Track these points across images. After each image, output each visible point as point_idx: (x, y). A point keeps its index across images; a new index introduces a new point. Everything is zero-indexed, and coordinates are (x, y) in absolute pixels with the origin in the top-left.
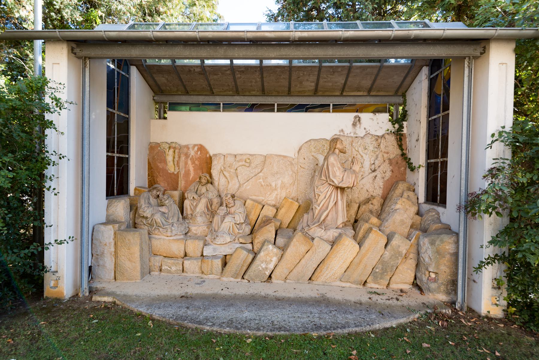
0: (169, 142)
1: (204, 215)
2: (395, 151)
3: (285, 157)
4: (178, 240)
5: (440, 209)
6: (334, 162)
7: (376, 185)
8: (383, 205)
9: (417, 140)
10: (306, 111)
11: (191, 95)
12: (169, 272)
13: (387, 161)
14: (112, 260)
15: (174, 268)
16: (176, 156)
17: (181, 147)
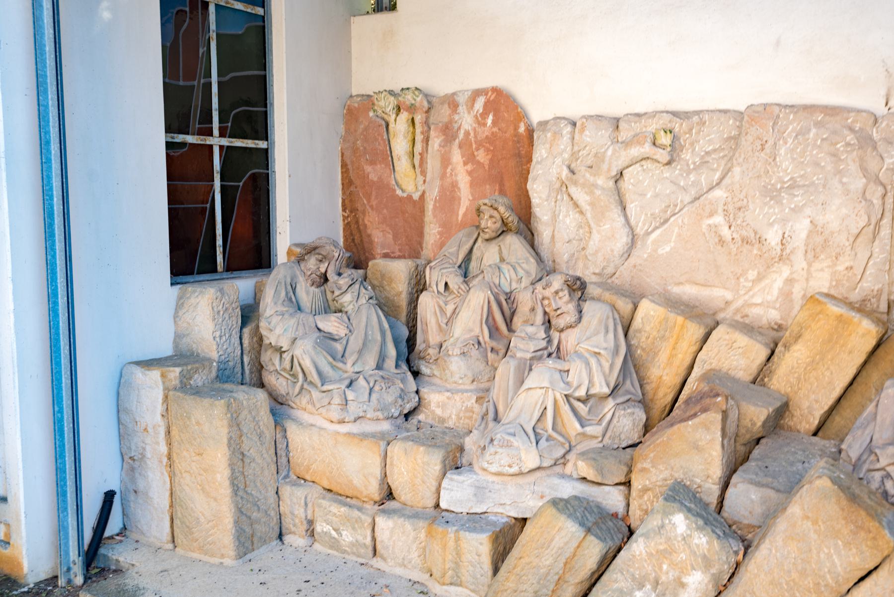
0: (397, 88)
1: (475, 353)
3: (831, 111)
4: (364, 436)
12: (334, 544)
14: (165, 482)
15: (347, 537)
16: (419, 138)
17: (431, 103)
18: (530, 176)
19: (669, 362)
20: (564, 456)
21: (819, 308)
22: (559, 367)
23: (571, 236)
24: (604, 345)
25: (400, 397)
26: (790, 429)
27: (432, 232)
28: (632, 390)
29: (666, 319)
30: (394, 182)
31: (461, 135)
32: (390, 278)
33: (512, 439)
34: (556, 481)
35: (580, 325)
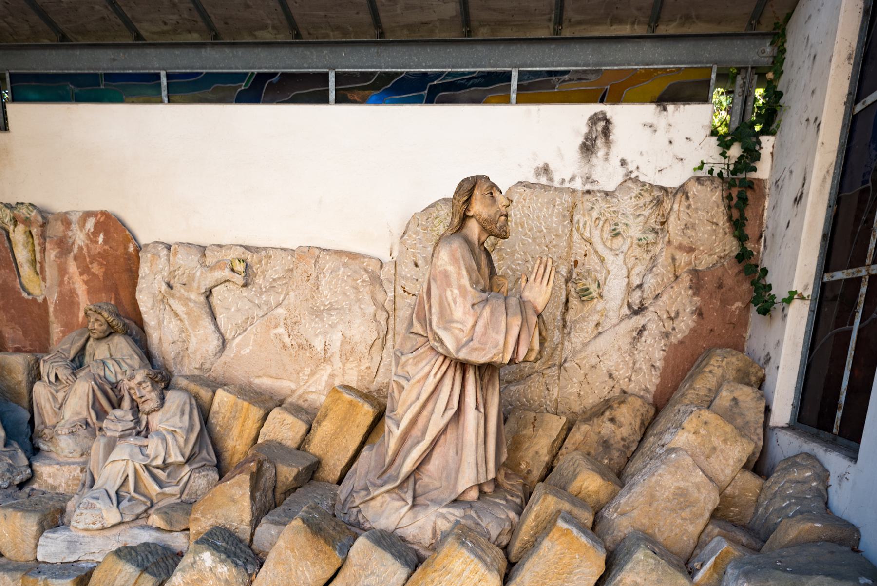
0: (13, 202)
1: (83, 432)
2: (714, 243)
3: (353, 256)
5: (835, 461)
6: (451, 268)
7: (640, 357)
8: (647, 427)
9: (798, 200)
10: (430, 100)
11: (74, 47)
13: (686, 279)
17: (45, 217)
18: (138, 288)
19: (240, 436)
20: (146, 511)
21: (337, 396)
22: (139, 443)
23: (176, 339)
24: (180, 425)
25: (8, 470)
26: (323, 480)
27: (56, 329)
28: (208, 457)
29: (236, 404)
30: (19, 286)
31: (76, 249)
32: (9, 369)
33: (95, 502)
34: (136, 531)
35: (162, 410)
